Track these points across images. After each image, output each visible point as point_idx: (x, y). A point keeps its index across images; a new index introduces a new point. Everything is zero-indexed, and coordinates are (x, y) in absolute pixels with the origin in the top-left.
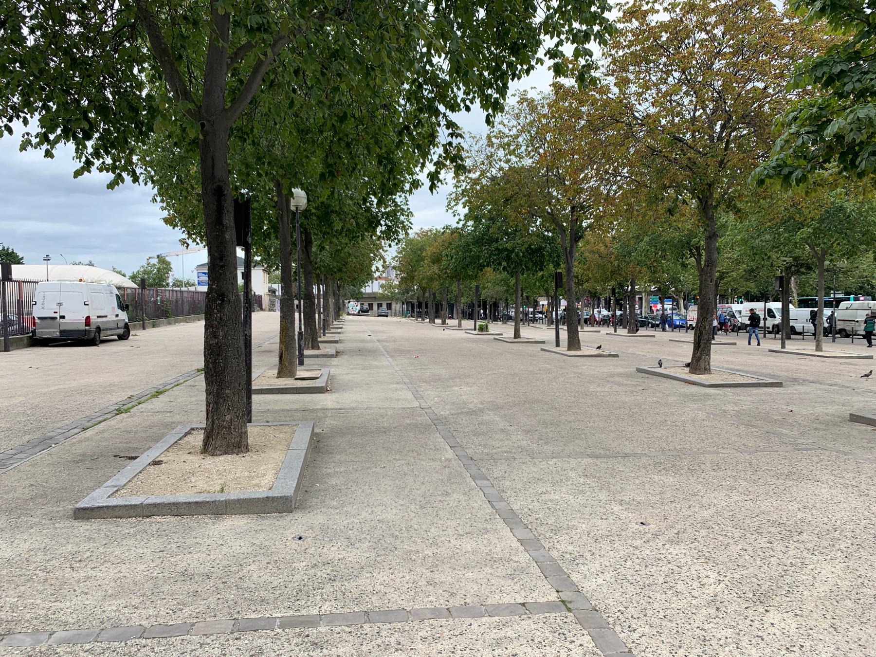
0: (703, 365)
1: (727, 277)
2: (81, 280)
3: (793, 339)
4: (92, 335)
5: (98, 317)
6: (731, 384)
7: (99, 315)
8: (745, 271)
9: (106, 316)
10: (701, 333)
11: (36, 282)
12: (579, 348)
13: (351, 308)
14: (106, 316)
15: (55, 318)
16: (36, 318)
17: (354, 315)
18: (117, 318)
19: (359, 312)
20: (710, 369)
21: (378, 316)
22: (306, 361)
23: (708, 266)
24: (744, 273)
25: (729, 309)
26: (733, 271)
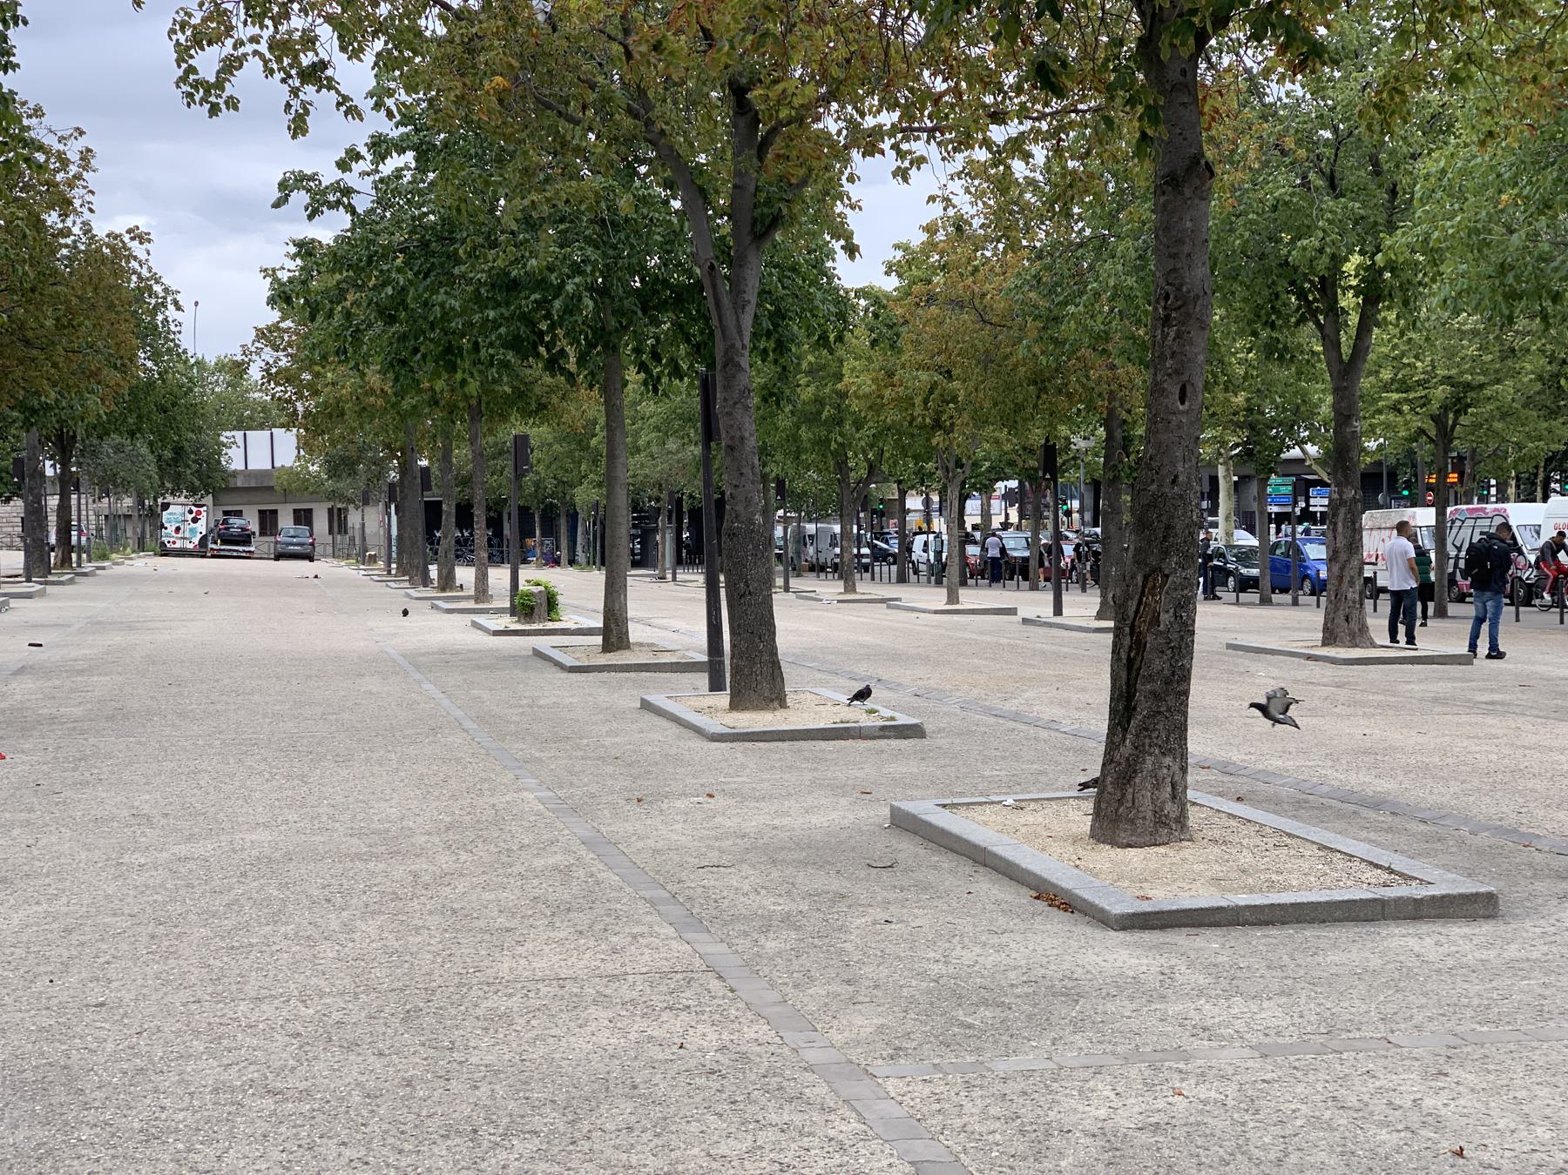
3: (1244, 604)
6: (1238, 910)
10: (1138, 645)
12: (777, 699)
13: (171, 529)
17: (182, 553)
19: (203, 541)
20: (1181, 819)
21: (278, 557)
23: (1166, 321)
24: (1538, 386)
26: (1498, 381)
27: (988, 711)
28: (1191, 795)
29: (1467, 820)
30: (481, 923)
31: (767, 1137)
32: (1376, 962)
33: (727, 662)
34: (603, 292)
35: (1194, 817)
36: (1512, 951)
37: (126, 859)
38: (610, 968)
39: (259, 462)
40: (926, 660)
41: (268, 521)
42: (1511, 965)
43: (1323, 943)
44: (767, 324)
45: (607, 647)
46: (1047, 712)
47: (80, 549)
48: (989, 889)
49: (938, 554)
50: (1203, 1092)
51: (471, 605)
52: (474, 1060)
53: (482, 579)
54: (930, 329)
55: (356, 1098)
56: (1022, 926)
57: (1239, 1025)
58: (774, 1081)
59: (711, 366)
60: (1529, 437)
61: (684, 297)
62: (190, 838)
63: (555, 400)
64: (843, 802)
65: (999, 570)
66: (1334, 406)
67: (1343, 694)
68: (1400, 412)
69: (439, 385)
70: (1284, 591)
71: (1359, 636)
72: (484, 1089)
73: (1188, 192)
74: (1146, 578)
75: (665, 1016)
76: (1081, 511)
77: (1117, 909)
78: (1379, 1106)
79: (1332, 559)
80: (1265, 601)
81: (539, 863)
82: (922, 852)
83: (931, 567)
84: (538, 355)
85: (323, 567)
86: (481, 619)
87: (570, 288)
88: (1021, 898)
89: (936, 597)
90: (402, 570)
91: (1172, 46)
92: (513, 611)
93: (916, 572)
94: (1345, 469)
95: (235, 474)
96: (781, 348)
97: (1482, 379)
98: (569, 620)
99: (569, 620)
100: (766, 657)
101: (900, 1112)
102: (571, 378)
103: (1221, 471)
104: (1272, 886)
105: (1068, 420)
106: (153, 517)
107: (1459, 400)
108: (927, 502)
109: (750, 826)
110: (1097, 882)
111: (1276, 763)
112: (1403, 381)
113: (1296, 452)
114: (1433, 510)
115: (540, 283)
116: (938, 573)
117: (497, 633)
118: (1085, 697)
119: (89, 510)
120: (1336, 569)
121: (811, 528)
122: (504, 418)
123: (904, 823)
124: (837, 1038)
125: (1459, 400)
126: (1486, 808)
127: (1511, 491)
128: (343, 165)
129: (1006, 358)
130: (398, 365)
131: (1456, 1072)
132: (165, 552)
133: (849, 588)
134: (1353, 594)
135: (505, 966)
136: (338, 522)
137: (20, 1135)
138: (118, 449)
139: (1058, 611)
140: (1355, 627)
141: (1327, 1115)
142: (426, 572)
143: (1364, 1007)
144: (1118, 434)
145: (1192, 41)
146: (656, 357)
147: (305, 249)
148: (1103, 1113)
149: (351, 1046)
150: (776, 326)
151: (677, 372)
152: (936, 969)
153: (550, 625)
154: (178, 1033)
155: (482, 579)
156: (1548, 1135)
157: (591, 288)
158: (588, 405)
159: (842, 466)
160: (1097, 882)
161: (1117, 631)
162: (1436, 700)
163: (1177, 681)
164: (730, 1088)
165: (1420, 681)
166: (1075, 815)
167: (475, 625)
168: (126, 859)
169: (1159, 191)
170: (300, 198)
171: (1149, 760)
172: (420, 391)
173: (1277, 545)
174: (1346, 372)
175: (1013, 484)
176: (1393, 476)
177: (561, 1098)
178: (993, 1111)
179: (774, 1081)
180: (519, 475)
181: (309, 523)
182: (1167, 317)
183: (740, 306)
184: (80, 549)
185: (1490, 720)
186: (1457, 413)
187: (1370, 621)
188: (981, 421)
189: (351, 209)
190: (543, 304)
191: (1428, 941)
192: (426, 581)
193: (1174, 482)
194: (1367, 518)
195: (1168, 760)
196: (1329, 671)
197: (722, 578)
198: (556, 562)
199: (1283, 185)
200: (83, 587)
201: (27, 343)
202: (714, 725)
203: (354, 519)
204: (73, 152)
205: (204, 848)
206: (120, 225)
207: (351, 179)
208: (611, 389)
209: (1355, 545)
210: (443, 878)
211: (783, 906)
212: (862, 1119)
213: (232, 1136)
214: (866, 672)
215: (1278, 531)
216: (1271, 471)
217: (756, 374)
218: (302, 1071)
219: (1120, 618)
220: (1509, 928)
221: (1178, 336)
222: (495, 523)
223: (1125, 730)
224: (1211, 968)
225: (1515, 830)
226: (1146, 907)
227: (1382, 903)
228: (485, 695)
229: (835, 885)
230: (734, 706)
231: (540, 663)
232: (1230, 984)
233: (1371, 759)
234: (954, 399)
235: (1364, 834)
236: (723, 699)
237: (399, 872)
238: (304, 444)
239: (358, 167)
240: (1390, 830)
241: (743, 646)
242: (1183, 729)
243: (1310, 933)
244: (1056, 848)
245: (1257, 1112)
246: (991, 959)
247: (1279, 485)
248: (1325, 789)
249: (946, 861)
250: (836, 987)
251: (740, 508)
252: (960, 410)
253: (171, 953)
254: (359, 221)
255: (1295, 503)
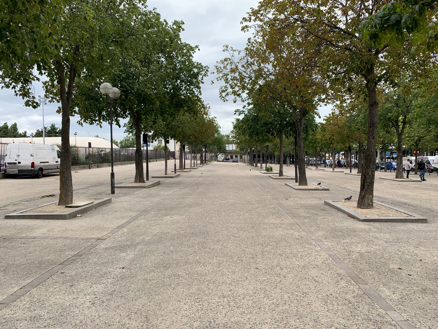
0: (366, 201)
1: (423, 140)
2: (30, 143)
4: (36, 173)
5: (41, 163)
6: (382, 219)
7: (41, 161)
8: (434, 136)
9: (48, 162)
10: (365, 177)
11: (8, 144)
12: (306, 184)
13: (219, 158)
14: (48, 162)
15: (16, 163)
16: (7, 163)
18: (57, 163)
20: (372, 205)
22: (116, 191)
23: (370, 127)
25: (426, 159)
27: (339, 187)
28: (374, 201)
29: (421, 207)
30: (262, 215)
31: (306, 249)
32: (406, 229)
33: (298, 178)
34: (280, 124)
35: (374, 205)
36: (430, 228)
37: (214, 203)
38: (281, 222)
39: (231, 149)
40: (329, 179)
41: (232, 157)
42: (430, 231)
43: (396, 225)
44: (305, 128)
45: (280, 176)
46: (349, 188)
47: (207, 161)
48: (340, 214)
49: (331, 163)
50: (376, 247)
51: (260, 169)
52: (262, 234)
53: (261, 165)
54: (331, 129)
55: (246, 238)
56: (346, 220)
57: (382, 237)
58: (307, 241)
59: (296, 134)
60: (432, 145)
61: (292, 125)
62: (222, 200)
63: (272, 140)
64: (317, 200)
65: (339, 165)
66: (398, 140)
67: (399, 186)
68: (409, 141)
69: (256, 138)
70: (389, 170)
71: (402, 177)
72: (264, 238)
73: (374, 107)
74: (367, 167)
75: (290, 230)
76: (354, 157)
77: (362, 218)
78: (406, 252)
79: (397, 165)
80: (385, 171)
81: (270, 207)
82: (329, 208)
83: (330, 165)
84: (270, 133)
85: (239, 163)
86: (261, 171)
87: (275, 123)
88: (346, 216)
89: (331, 170)
90: (250, 164)
91: (371, 85)
92: (266, 170)
93: (327, 166)
94: (400, 150)
95: (227, 150)
96: (307, 132)
97: (423, 136)
98: (274, 172)
99: (274, 172)
100: (304, 178)
101: (327, 247)
102: (275, 137)
103: (378, 151)
104: (387, 216)
105: (352, 142)
106: (217, 156)
107: (419, 139)
108: (329, 155)
109: (302, 203)
110: (358, 214)
111: (388, 197)
112: (410, 136)
113: (391, 148)
114: (415, 157)
115: (271, 123)
116: (331, 166)
117: (263, 173)
118: (356, 185)
119: (209, 155)
120: (398, 166)
121: (311, 159)
122: (265, 142)
123: (326, 203)
124: (317, 235)
125: (419, 139)
126: (425, 205)
127: (429, 154)
128: (244, 108)
129: (342, 133)
130: (250, 136)
131: (420, 247)
132: (218, 161)
133: (317, 168)
134: (401, 170)
135: (266, 221)
136: (241, 157)
137: (201, 240)
138: (212, 147)
139: (351, 172)
140: (401, 175)
141: (397, 252)
142: (253, 164)
143: (404, 236)
144: (361, 145)
145: (374, 84)
146: (288, 133)
147: (238, 120)
148: (359, 249)
149: (245, 231)
150: (306, 128)
151: (291, 136)
152: (332, 226)
153: (271, 172)
154: (221, 227)
155: (261, 165)
156: (437, 259)
157: (279, 124)
158: (277, 140)
159: (316, 150)
160: (358, 214)
161: (362, 175)
162: (415, 188)
163: (372, 183)
164: (300, 241)
165: (413, 184)
166: (355, 204)
167: (260, 172)
168: (214, 203)
169: (369, 107)
170: (238, 113)
171: (367, 195)
172: (253, 139)
173: (388, 162)
174: (400, 135)
175: (343, 152)
176: (408, 152)
177: (275, 241)
178: (341, 248)
179: (307, 241)
180: (267, 151)
181: (237, 157)
182: (371, 126)
183: (301, 126)
184: (207, 161)
185: (425, 191)
186: (419, 142)
187: (404, 175)
188: (338, 143)
189: (245, 114)
190: (272, 126)
191: (415, 226)
192: (253, 166)
193: (372, 152)
194: (404, 158)
195: (370, 196)
196: (397, 182)
197: (298, 166)
198: (272, 163)
199: (389, 105)
200: (208, 166)
201: (202, 133)
202: (296, 188)
203: (243, 157)
204: (208, 106)
205: (224, 202)
206: (213, 116)
207: (244, 110)
208: (281, 138)
209: (401, 162)
210: (257, 208)
211: (308, 215)
212: (321, 248)
213: (229, 242)
214: (320, 180)
215: (388, 160)
216: (387, 151)
217: (303, 135)
218: (238, 234)
219: (362, 173)
220: (429, 225)
221: (372, 129)
222: (263, 157)
223: (363, 191)
224: (377, 228)
225: (430, 209)
226: (366, 218)
227: (407, 219)
228: (262, 182)
229: (316, 212)
230: (299, 185)
231: (270, 178)
232: (381, 231)
233: (404, 197)
234: (334, 139)
235: (403, 208)
236: (298, 184)
237: (250, 207)
238: (237, 147)
239: (246, 108)
240: (408, 208)
241: (301, 176)
242: (373, 191)
243: (394, 224)
244: (351, 209)
245: (385, 251)
246: (341, 225)
247: (388, 153)
248: (396, 201)
249: (333, 210)
250: (316, 228)
251: (300, 156)
252: (335, 141)
253: (220, 216)
254: (246, 115)
255: (391, 156)
